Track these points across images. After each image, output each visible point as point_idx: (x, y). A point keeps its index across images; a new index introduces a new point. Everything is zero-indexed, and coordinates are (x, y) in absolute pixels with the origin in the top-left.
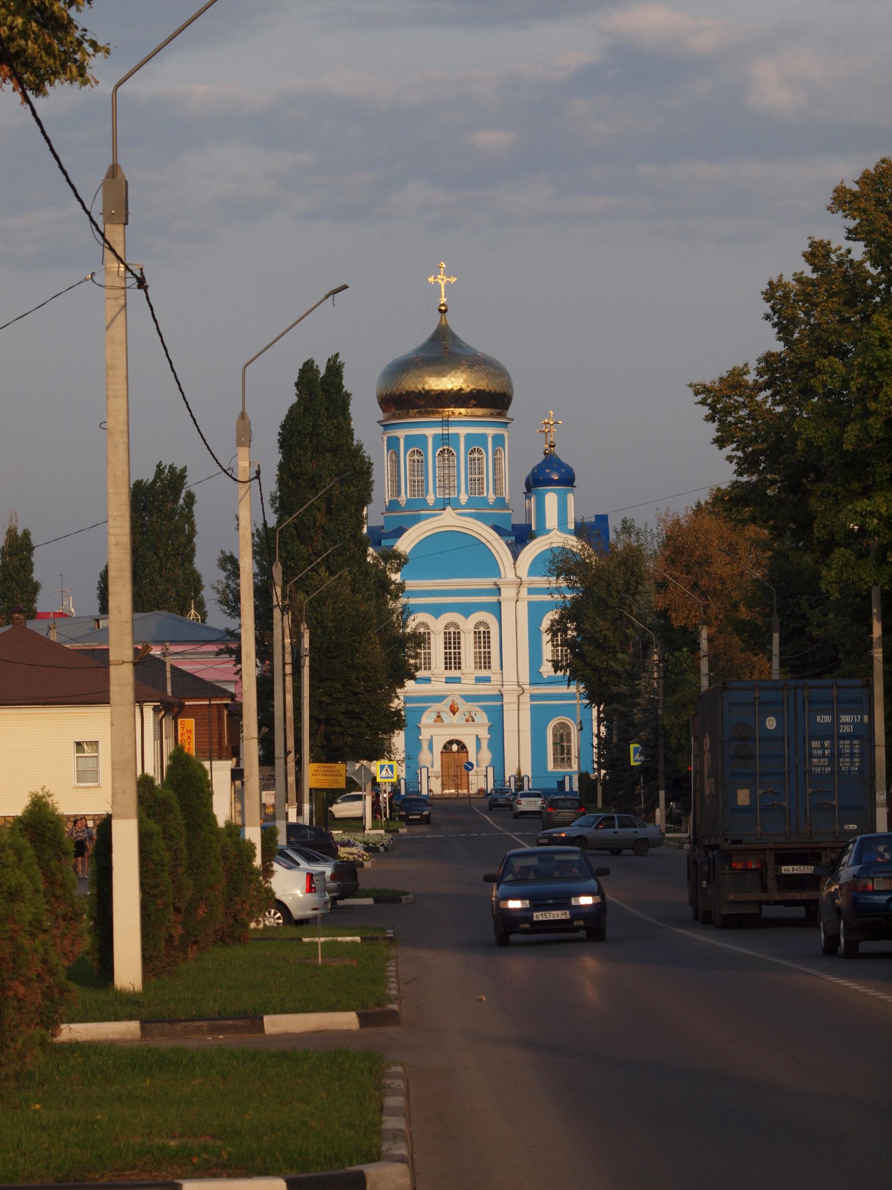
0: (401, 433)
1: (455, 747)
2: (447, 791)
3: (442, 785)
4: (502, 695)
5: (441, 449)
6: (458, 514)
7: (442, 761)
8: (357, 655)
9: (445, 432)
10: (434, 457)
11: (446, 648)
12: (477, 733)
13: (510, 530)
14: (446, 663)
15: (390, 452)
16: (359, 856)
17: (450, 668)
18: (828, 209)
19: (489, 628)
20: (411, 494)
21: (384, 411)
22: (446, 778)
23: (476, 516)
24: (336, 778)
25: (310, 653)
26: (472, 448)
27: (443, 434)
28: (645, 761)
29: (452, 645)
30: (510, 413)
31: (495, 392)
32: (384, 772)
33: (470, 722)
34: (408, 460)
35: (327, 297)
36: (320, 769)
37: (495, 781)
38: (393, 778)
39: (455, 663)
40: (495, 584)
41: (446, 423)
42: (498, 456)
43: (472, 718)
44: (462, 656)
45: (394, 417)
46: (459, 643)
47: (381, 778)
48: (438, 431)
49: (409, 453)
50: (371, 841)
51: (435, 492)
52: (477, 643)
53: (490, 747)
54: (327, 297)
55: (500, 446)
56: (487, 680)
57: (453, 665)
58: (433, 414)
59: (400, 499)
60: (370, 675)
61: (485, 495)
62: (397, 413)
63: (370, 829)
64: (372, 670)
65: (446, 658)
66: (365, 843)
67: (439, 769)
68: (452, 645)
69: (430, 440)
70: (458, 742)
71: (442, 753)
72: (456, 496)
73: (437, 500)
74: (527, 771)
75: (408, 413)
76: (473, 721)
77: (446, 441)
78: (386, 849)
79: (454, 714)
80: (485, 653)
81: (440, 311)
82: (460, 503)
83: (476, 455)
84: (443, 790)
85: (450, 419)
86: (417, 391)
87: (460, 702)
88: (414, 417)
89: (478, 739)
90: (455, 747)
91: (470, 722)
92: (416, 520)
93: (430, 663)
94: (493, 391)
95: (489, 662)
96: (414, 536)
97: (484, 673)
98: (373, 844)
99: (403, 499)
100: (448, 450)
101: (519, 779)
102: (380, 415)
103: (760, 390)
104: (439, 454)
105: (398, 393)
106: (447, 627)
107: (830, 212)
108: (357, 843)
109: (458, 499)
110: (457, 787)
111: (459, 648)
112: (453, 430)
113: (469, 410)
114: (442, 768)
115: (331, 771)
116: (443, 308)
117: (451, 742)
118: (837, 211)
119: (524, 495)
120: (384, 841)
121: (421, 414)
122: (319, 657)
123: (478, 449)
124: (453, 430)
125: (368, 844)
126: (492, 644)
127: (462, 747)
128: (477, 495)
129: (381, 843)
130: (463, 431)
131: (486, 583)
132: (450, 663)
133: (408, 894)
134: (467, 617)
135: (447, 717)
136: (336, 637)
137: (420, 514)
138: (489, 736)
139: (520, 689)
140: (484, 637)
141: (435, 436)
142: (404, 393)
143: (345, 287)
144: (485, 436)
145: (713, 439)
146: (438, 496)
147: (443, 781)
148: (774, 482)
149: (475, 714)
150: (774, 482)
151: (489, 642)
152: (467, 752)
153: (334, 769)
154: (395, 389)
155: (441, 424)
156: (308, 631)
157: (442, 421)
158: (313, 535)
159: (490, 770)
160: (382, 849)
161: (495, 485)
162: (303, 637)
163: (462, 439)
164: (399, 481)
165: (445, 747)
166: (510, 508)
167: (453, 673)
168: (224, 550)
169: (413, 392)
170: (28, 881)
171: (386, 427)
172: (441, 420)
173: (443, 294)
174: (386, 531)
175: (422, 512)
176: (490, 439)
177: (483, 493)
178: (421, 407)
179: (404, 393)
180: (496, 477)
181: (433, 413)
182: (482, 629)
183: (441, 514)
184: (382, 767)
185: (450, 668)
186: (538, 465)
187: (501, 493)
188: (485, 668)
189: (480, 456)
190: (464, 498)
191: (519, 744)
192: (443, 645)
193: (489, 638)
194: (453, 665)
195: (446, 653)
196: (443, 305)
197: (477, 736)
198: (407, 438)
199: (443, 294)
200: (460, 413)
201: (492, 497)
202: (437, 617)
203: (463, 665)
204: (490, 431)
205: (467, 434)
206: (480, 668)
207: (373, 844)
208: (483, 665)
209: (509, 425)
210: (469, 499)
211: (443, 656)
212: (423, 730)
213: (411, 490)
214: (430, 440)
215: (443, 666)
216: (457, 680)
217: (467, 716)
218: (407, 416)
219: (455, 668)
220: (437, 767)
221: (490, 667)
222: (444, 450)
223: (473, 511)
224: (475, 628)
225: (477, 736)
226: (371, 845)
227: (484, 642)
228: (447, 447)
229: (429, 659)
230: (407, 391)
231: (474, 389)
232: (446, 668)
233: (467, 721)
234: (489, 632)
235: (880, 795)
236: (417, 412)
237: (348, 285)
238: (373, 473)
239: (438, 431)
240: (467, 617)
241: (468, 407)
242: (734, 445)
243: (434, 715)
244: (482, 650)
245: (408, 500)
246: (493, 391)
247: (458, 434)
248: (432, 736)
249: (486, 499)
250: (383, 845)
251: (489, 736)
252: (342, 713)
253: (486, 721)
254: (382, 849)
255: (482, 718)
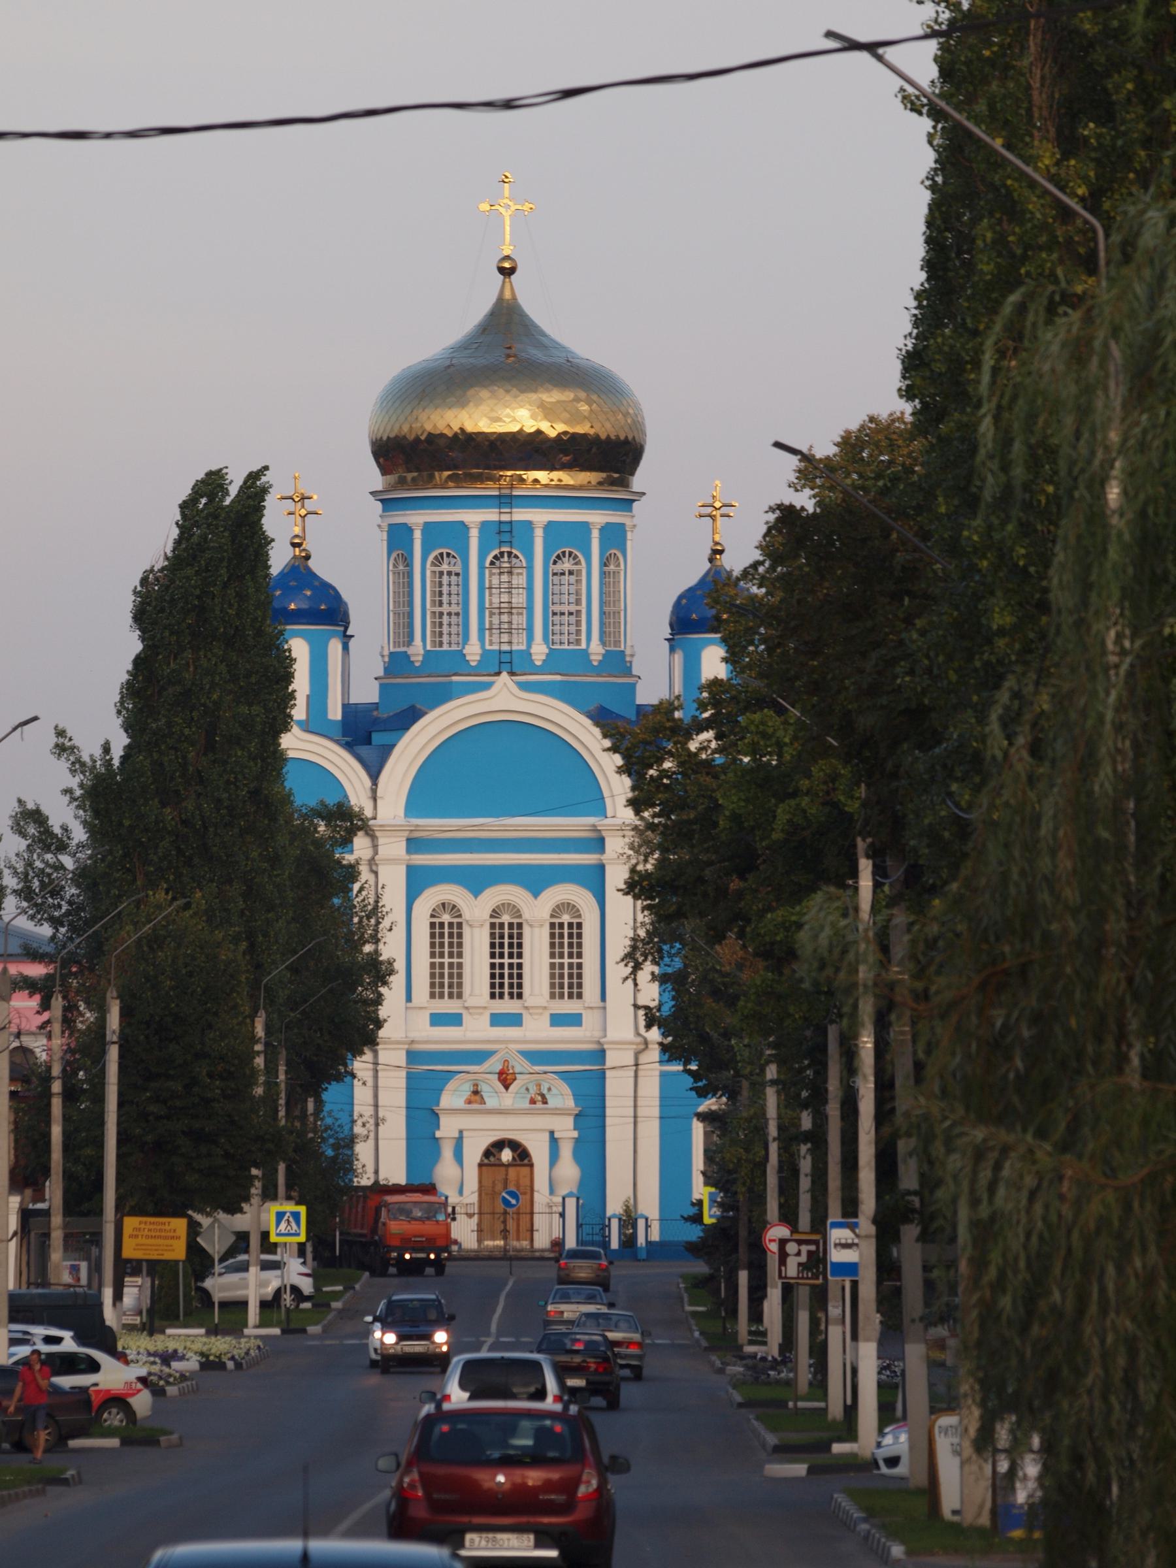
0: (417, 518)
1: (507, 1155)
2: (489, 1243)
3: (480, 1230)
4: (603, 1051)
5: (496, 552)
6: (524, 687)
7: (480, 1182)
8: (211, 1035)
9: (506, 518)
10: (481, 568)
11: (493, 955)
12: (551, 1127)
13: (634, 718)
14: (493, 986)
15: (394, 555)
16: (160, 1378)
17: (501, 996)
18: (790, 486)
19: (580, 916)
20: (433, 642)
21: (385, 471)
22: (487, 1217)
23: (565, 693)
24: (169, 1242)
25: (120, 1038)
26: (559, 552)
27: (500, 522)
28: (723, 1217)
29: (506, 950)
30: (638, 481)
31: (608, 437)
32: (283, 1226)
33: (539, 1105)
34: (428, 573)
35: (15, 729)
36: (143, 1226)
37: (579, 1226)
38: (298, 1235)
39: (511, 986)
40: (594, 829)
41: (505, 501)
42: (612, 567)
43: (543, 1096)
44: (526, 971)
45: (402, 483)
46: (520, 945)
47: (278, 1235)
48: (491, 515)
49: (431, 558)
50: (213, 1351)
51: (481, 639)
52: (555, 948)
53: (577, 1156)
54: (15, 729)
55: (618, 549)
56: (574, 1020)
57: (506, 990)
58: (482, 482)
59: (410, 651)
60: (232, 1069)
61: (584, 646)
62: (410, 476)
63: (256, 1327)
64: (236, 1062)
65: (493, 976)
66: (202, 1354)
67: (474, 1198)
68: (506, 950)
69: (474, 533)
70: (514, 1145)
71: (481, 1165)
72: (523, 647)
73: (485, 654)
74: (650, 1206)
75: (432, 477)
76: (545, 1102)
77: (506, 537)
78: (239, 1366)
79: (507, 1087)
80: (571, 966)
81: (501, 270)
82: (532, 661)
83: (566, 565)
84: (480, 1241)
85: (515, 493)
86: (450, 434)
87: (520, 1065)
88: (443, 487)
89: (554, 1141)
90: (507, 1155)
91: (539, 1105)
92: (443, 695)
93: (460, 985)
94: (603, 437)
95: (580, 986)
96: (433, 730)
97: (567, 1006)
98: (216, 1357)
99: (417, 650)
100: (510, 554)
101: (629, 1219)
102: (375, 479)
103: (700, 730)
104: (492, 563)
105: (411, 437)
106: (495, 913)
107: (792, 489)
108: (190, 1354)
109: (527, 654)
110: (505, 1234)
111: (520, 956)
112: (520, 515)
113: (556, 475)
114: (480, 1195)
115: (161, 1230)
116: (507, 265)
117: (499, 1145)
118: (803, 487)
119: (667, 643)
120: (235, 1352)
121: (457, 481)
122: (147, 1037)
123: (570, 554)
124: (520, 515)
125: (207, 1356)
126: (586, 950)
127: (522, 1155)
128: (566, 647)
129: (229, 1355)
130: (539, 517)
131: (575, 824)
132: (502, 985)
133: (171, 1433)
134: (536, 895)
135: (495, 1097)
136: (177, 1005)
137: (451, 683)
138: (575, 1134)
139: (639, 1039)
140: (571, 936)
141: (484, 525)
142: (423, 438)
143: (35, 719)
144: (585, 527)
145: (627, 801)
146: (488, 647)
147: (479, 1225)
148: (710, 863)
149: (549, 1089)
150: (710, 863)
151: (580, 945)
152: (531, 1166)
153: (167, 1227)
154: (406, 429)
155: (497, 502)
156: (118, 1002)
157: (499, 496)
158: (181, 788)
159: (571, 1204)
160: (230, 1365)
161: (602, 624)
162: (109, 1012)
163: (539, 533)
164: (411, 615)
165: (487, 1153)
166: (634, 672)
167: (507, 1006)
168: (23, 799)
169: (442, 435)
170: (985, 806)
171: (388, 504)
172: (496, 493)
173: (508, 237)
174: (383, 714)
175: (455, 678)
176: (595, 534)
177: (578, 642)
178: (456, 467)
179: (423, 438)
180: (606, 609)
181: (480, 479)
182: (566, 918)
183: (487, 686)
184: (280, 1216)
185: (501, 996)
186: (690, 590)
187: (617, 643)
188: (571, 996)
189: (575, 568)
190: (539, 651)
191: (635, 1151)
192: (486, 950)
193: (580, 936)
194: (506, 990)
195: (493, 966)
196: (507, 258)
197: (552, 1133)
198: (428, 527)
199: (508, 237)
200: (536, 481)
201: (596, 650)
202: (476, 893)
203: (526, 990)
204: (597, 518)
205: (550, 522)
206: (562, 996)
207: (216, 1357)
208: (566, 990)
209: (635, 504)
210: (552, 653)
211: (487, 971)
212: (444, 1120)
213: (433, 632)
214: (474, 533)
215: (486, 990)
216: (515, 1020)
217: (533, 1090)
218: (429, 482)
219: (511, 995)
220: (471, 1196)
221: (580, 996)
222: (502, 554)
223: (558, 678)
224: (552, 916)
225: (552, 1133)
226: (212, 1358)
227: (571, 945)
228: (508, 549)
229: (460, 976)
230: (430, 434)
231: (565, 433)
232: (493, 996)
233: (533, 1102)
234: (579, 925)
235: (833, 1306)
236: (449, 477)
237: (39, 716)
238: (296, 675)
239: (491, 515)
240: (536, 895)
241: (552, 468)
242: (657, 809)
243: (467, 1088)
244: (566, 961)
245: (427, 652)
246: (603, 437)
247: (530, 523)
248: (461, 1132)
249: (585, 653)
250: (233, 1358)
251: (575, 1134)
252: (183, 1132)
253: (570, 1103)
254: (230, 1365)
255: (562, 1097)
